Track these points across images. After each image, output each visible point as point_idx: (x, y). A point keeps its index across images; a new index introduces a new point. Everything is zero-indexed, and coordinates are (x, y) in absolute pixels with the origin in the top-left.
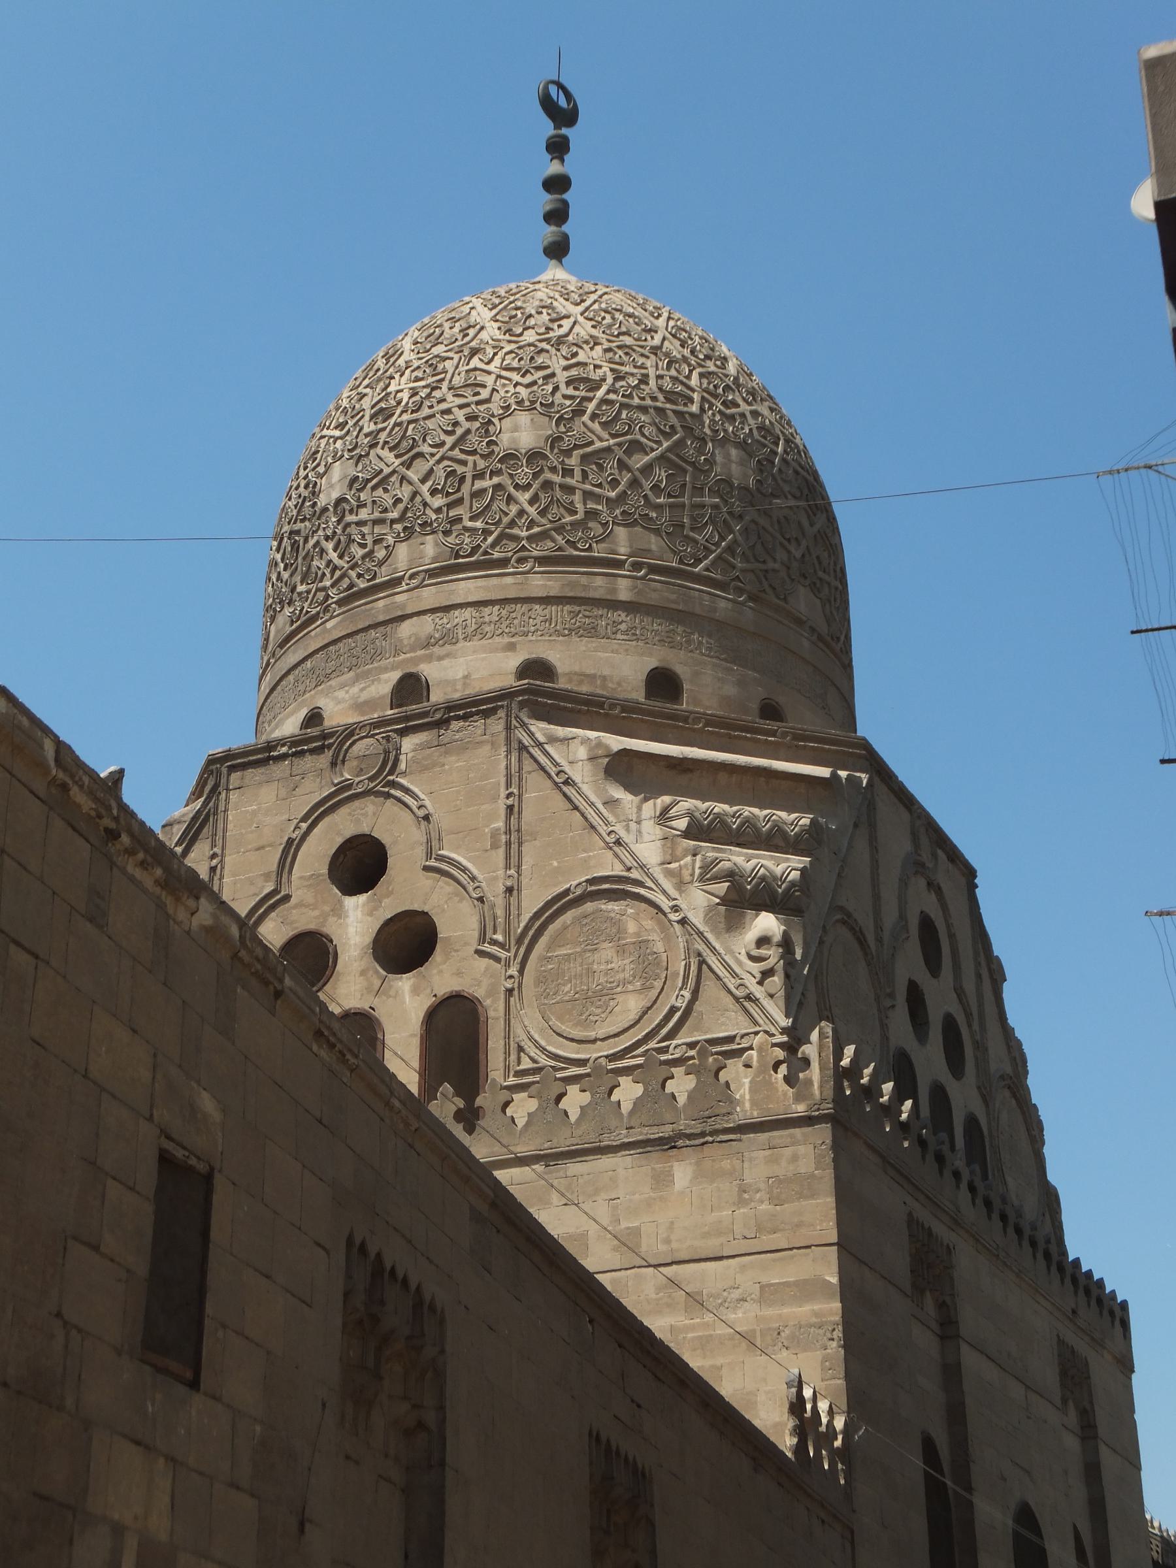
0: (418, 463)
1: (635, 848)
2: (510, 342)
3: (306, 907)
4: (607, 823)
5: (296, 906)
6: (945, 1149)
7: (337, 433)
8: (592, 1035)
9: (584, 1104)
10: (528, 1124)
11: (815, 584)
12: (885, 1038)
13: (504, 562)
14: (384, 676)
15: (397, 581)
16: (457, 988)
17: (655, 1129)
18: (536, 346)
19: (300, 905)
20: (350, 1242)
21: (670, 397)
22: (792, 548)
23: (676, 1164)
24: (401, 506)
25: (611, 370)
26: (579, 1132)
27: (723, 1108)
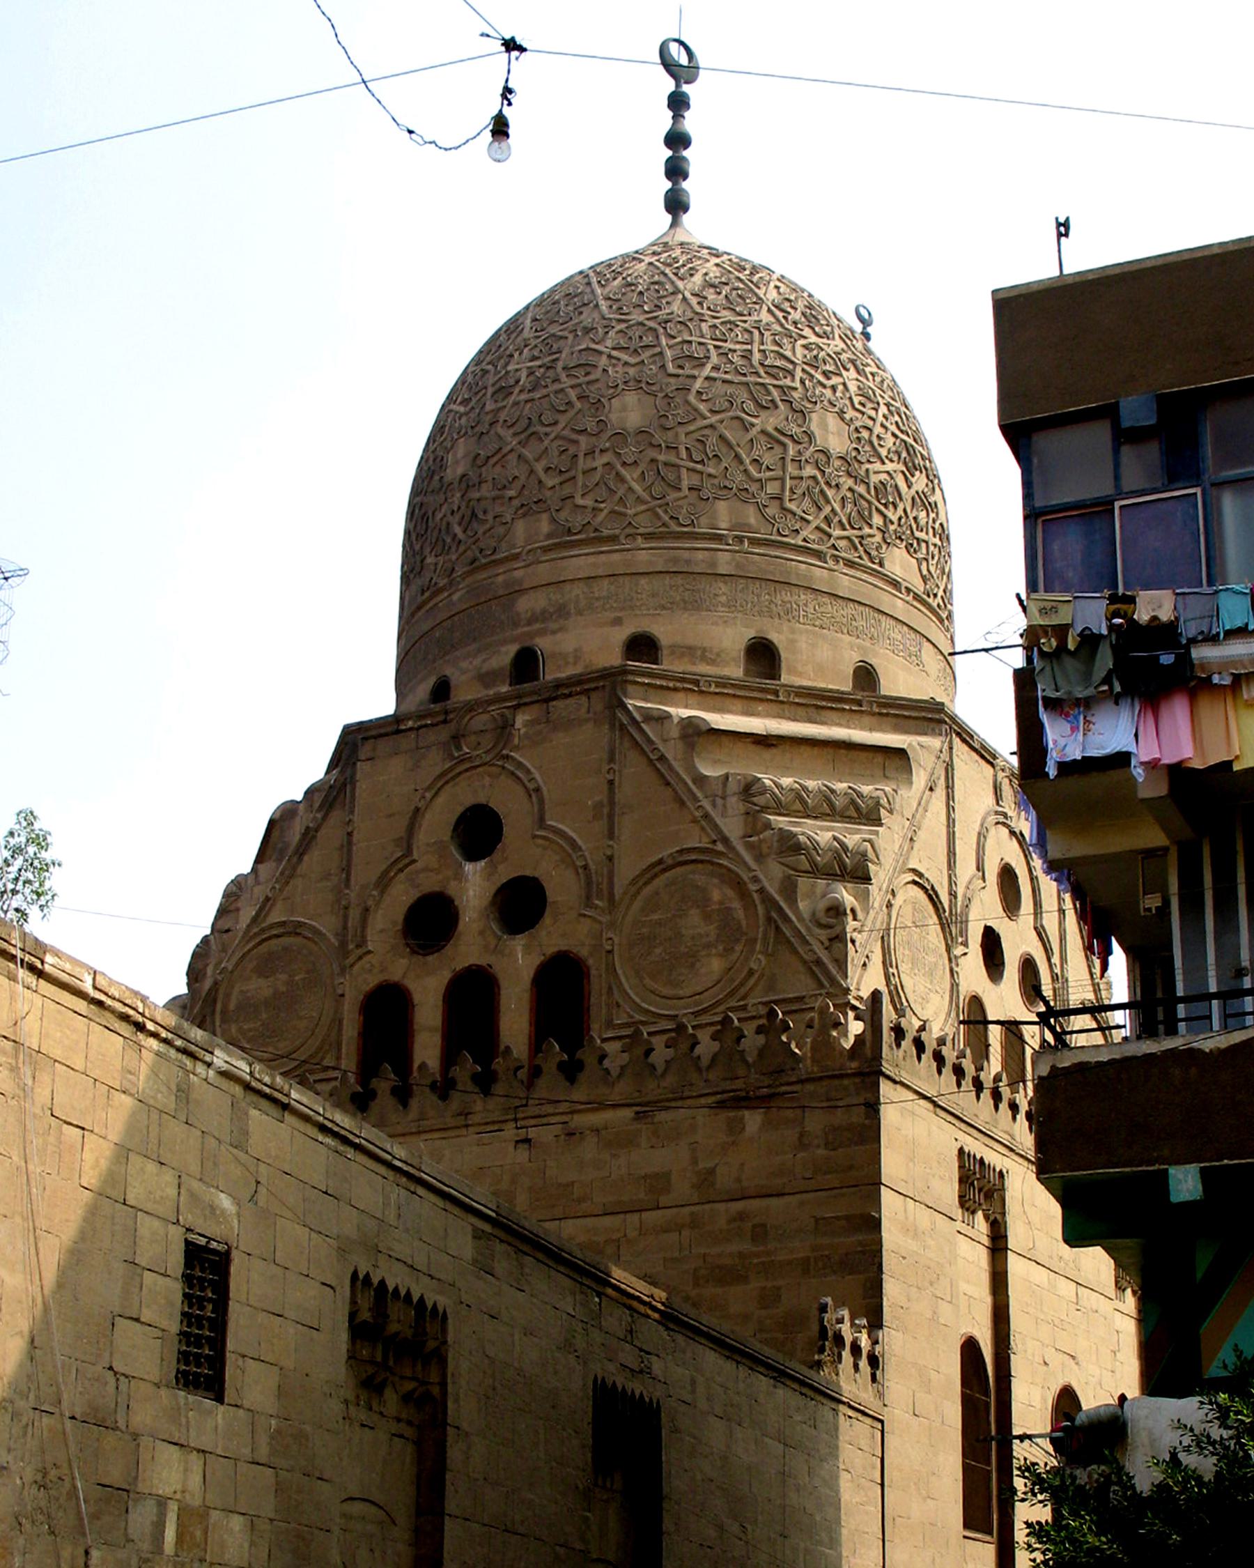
0: (533, 441)
1: (719, 821)
2: (620, 321)
4: (696, 799)
7: (462, 409)
9: (668, 1058)
10: (620, 1075)
11: (912, 545)
12: (954, 986)
13: (613, 539)
14: (504, 649)
15: (516, 557)
16: (564, 948)
17: (728, 1082)
18: (644, 325)
19: (426, 869)
20: (355, 1276)
21: (772, 371)
23: (746, 1113)
24: (518, 484)
25: (715, 347)
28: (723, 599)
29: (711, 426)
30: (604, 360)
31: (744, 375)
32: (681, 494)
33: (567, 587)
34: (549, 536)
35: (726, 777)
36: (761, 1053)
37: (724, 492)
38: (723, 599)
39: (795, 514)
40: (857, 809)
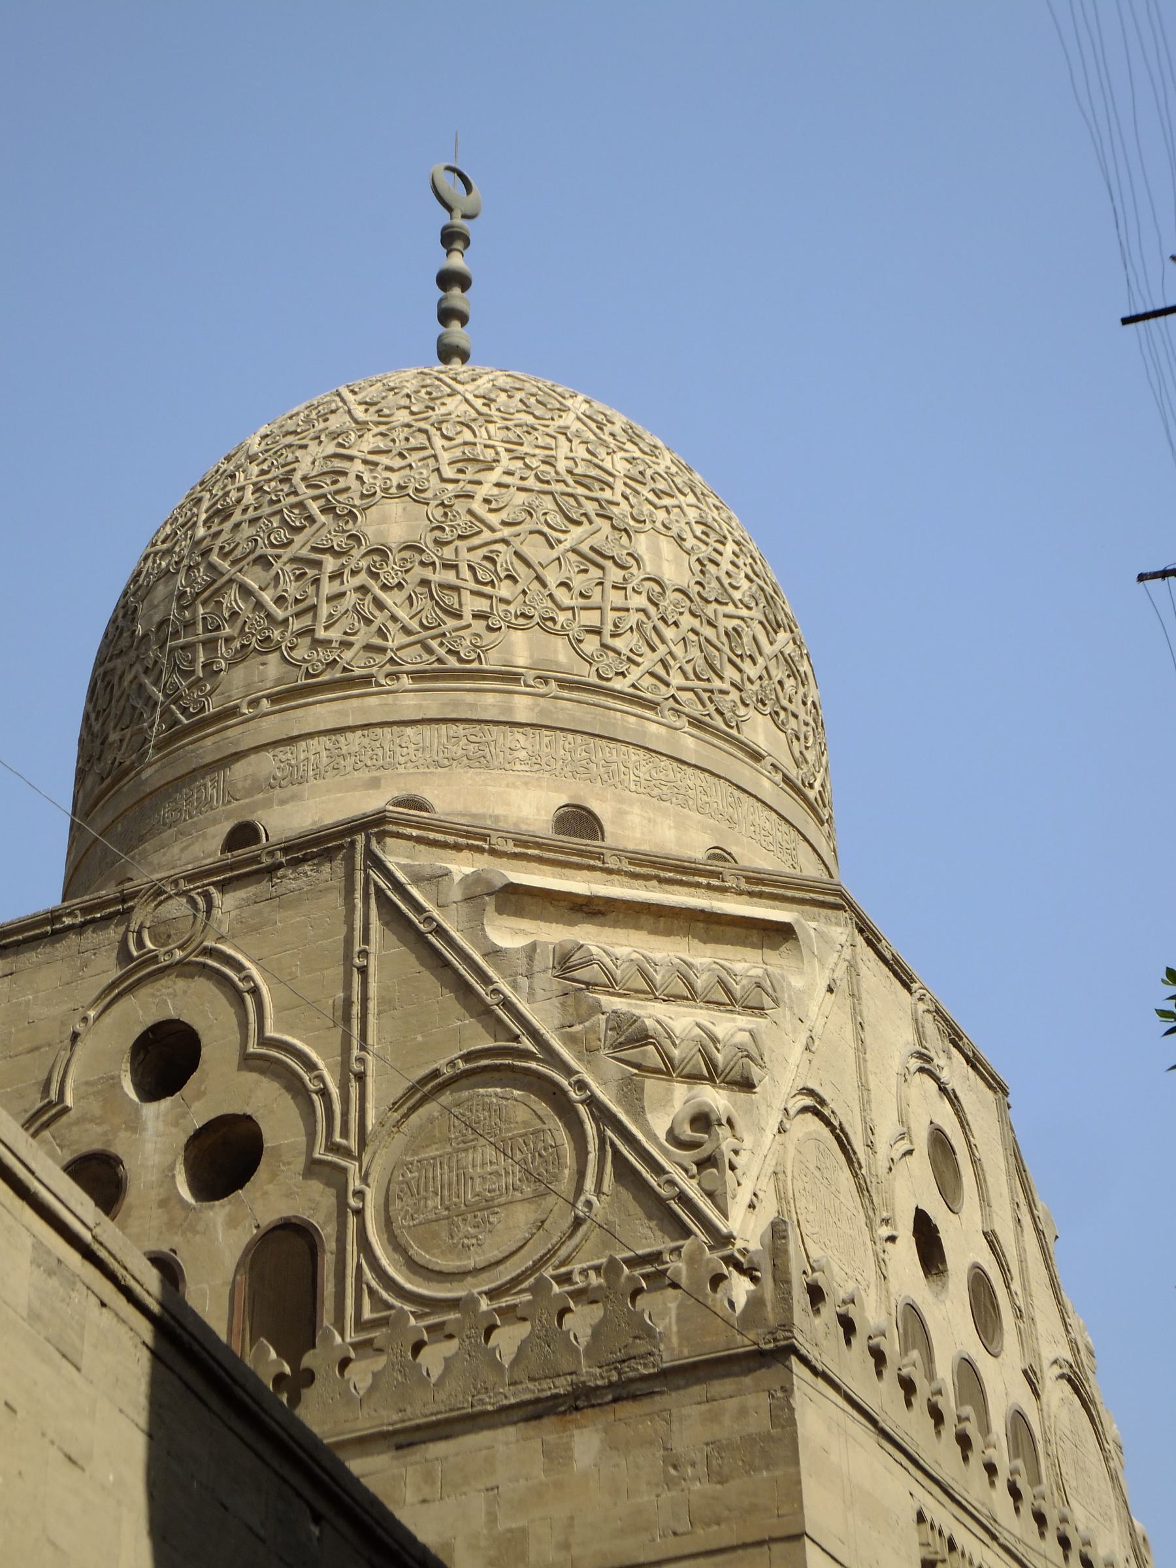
3: (92, 1121)
5: (77, 1122)
6: (972, 1429)
8: (470, 1264)
10: (372, 1388)
11: (777, 713)
13: (367, 680)
14: (211, 830)
16: (290, 1213)
22: (747, 666)
23: (576, 1432)
26: (442, 1396)
27: (642, 1347)
28: (522, 754)
29: (504, 541)
30: (358, 466)
31: (548, 482)
32: (463, 623)
33: (302, 745)
34: (279, 682)
35: (533, 946)
36: (597, 1332)
37: (521, 621)
38: (522, 754)
39: (619, 654)
40: (728, 991)
